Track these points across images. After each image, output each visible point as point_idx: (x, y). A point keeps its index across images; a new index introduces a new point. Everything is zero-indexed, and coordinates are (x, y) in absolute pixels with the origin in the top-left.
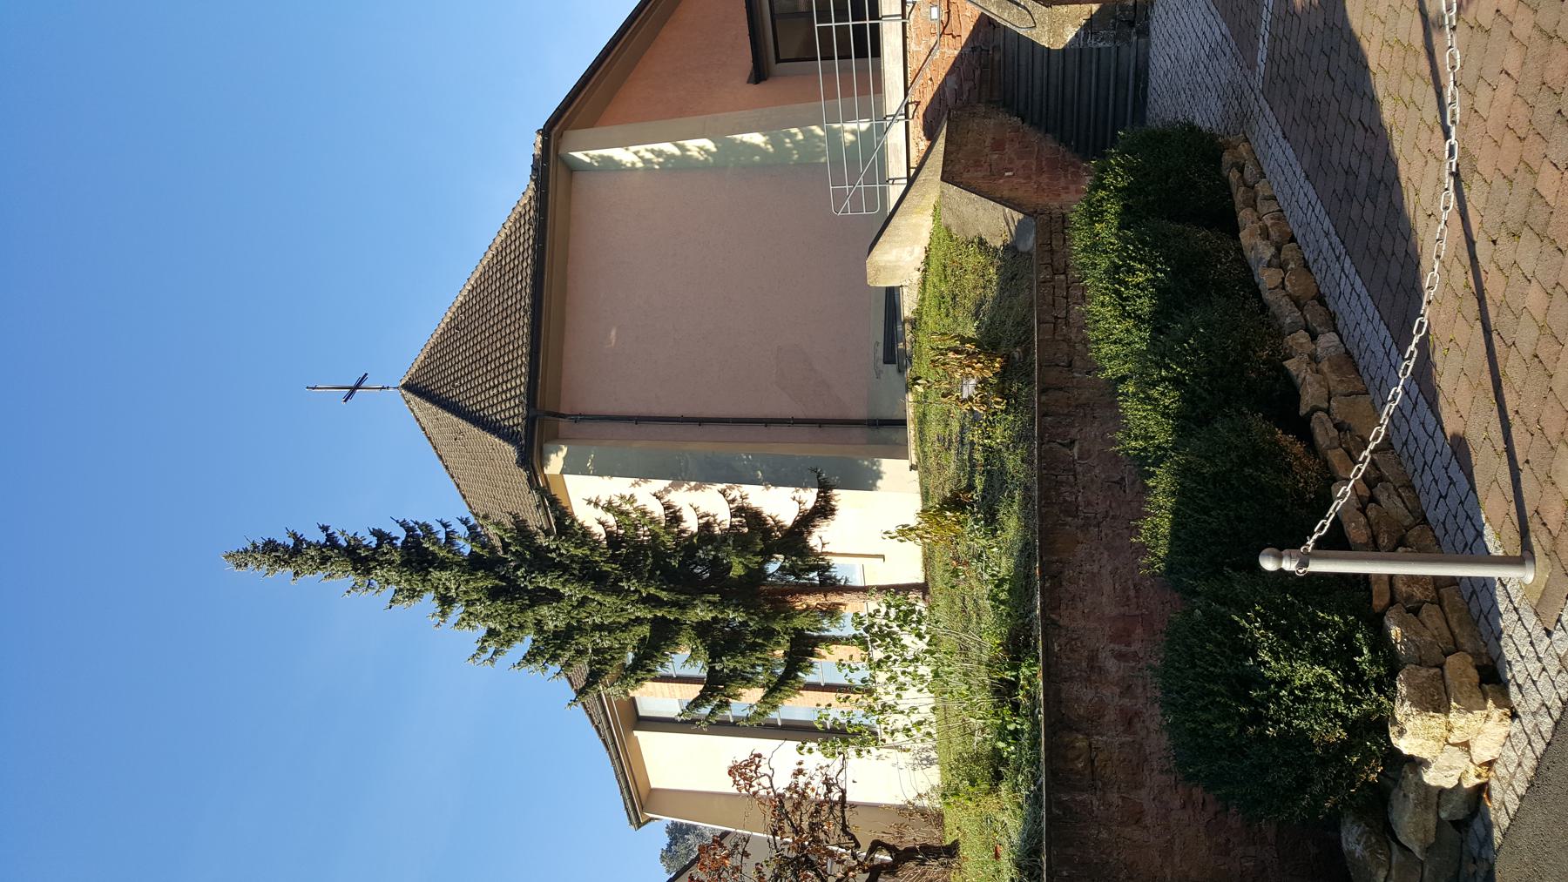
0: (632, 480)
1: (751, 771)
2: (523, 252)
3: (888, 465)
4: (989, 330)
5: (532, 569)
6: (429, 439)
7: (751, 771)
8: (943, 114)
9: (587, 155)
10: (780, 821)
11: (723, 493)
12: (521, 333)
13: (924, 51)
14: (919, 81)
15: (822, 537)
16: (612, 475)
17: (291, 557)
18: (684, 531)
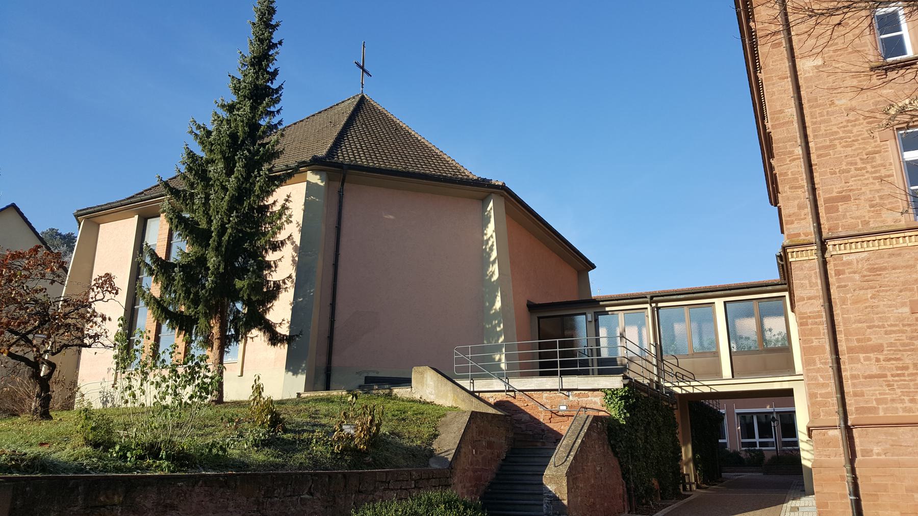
0: (301, 222)
1: (107, 288)
2: (444, 170)
3: (301, 379)
4: (383, 441)
5: (248, 159)
6: (331, 107)
7: (107, 288)
8: (508, 412)
9: (491, 209)
10: (74, 305)
11: (290, 277)
12: (393, 165)
13: (543, 401)
14: (527, 399)
15: (257, 337)
16: (304, 211)
17: (264, 22)
18: (266, 252)
